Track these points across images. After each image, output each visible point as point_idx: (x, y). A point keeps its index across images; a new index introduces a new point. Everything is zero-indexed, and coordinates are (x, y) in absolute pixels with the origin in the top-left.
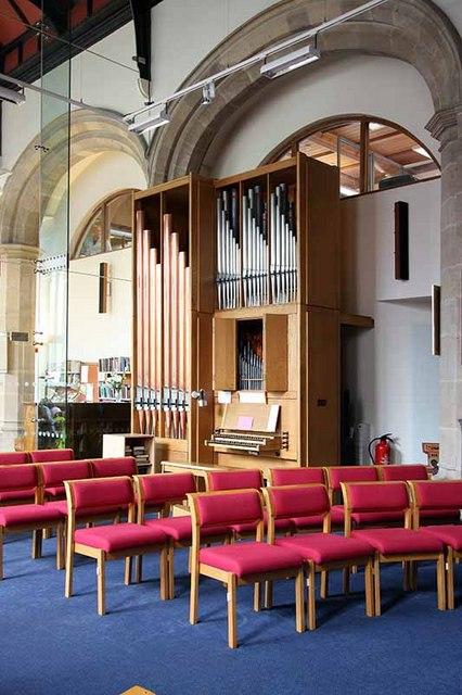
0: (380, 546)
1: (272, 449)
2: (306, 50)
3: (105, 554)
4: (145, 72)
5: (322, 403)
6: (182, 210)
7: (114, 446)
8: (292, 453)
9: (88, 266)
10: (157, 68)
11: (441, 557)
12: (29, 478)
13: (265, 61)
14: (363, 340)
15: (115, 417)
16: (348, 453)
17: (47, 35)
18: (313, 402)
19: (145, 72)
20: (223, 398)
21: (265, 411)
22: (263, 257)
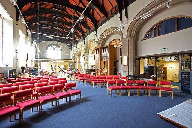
0: (140, 88)
1: (107, 74)
2: (151, 14)
3: (112, 90)
4: (97, 36)
5: (112, 69)
6: (99, 50)
7: (92, 73)
8: (108, 74)
9: (94, 55)
10: (123, 20)
11: (159, 90)
12: (123, 82)
13: (142, 17)
14: (118, 63)
15: (93, 71)
16: (116, 74)
17: (105, 18)
18: (111, 69)
19: (97, 36)
20: (103, 69)
21: (106, 70)
22: (106, 54)
